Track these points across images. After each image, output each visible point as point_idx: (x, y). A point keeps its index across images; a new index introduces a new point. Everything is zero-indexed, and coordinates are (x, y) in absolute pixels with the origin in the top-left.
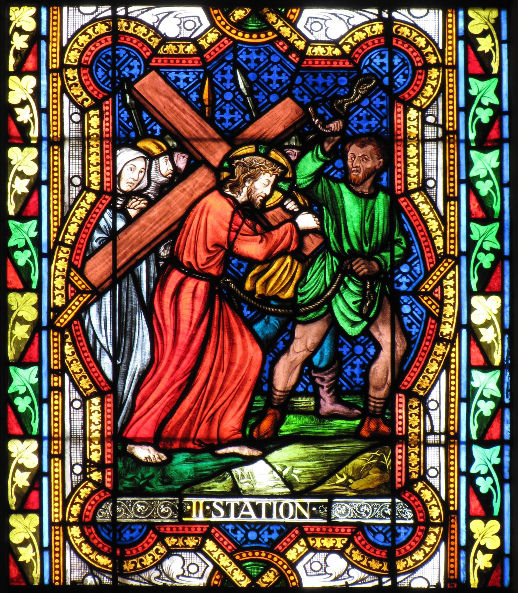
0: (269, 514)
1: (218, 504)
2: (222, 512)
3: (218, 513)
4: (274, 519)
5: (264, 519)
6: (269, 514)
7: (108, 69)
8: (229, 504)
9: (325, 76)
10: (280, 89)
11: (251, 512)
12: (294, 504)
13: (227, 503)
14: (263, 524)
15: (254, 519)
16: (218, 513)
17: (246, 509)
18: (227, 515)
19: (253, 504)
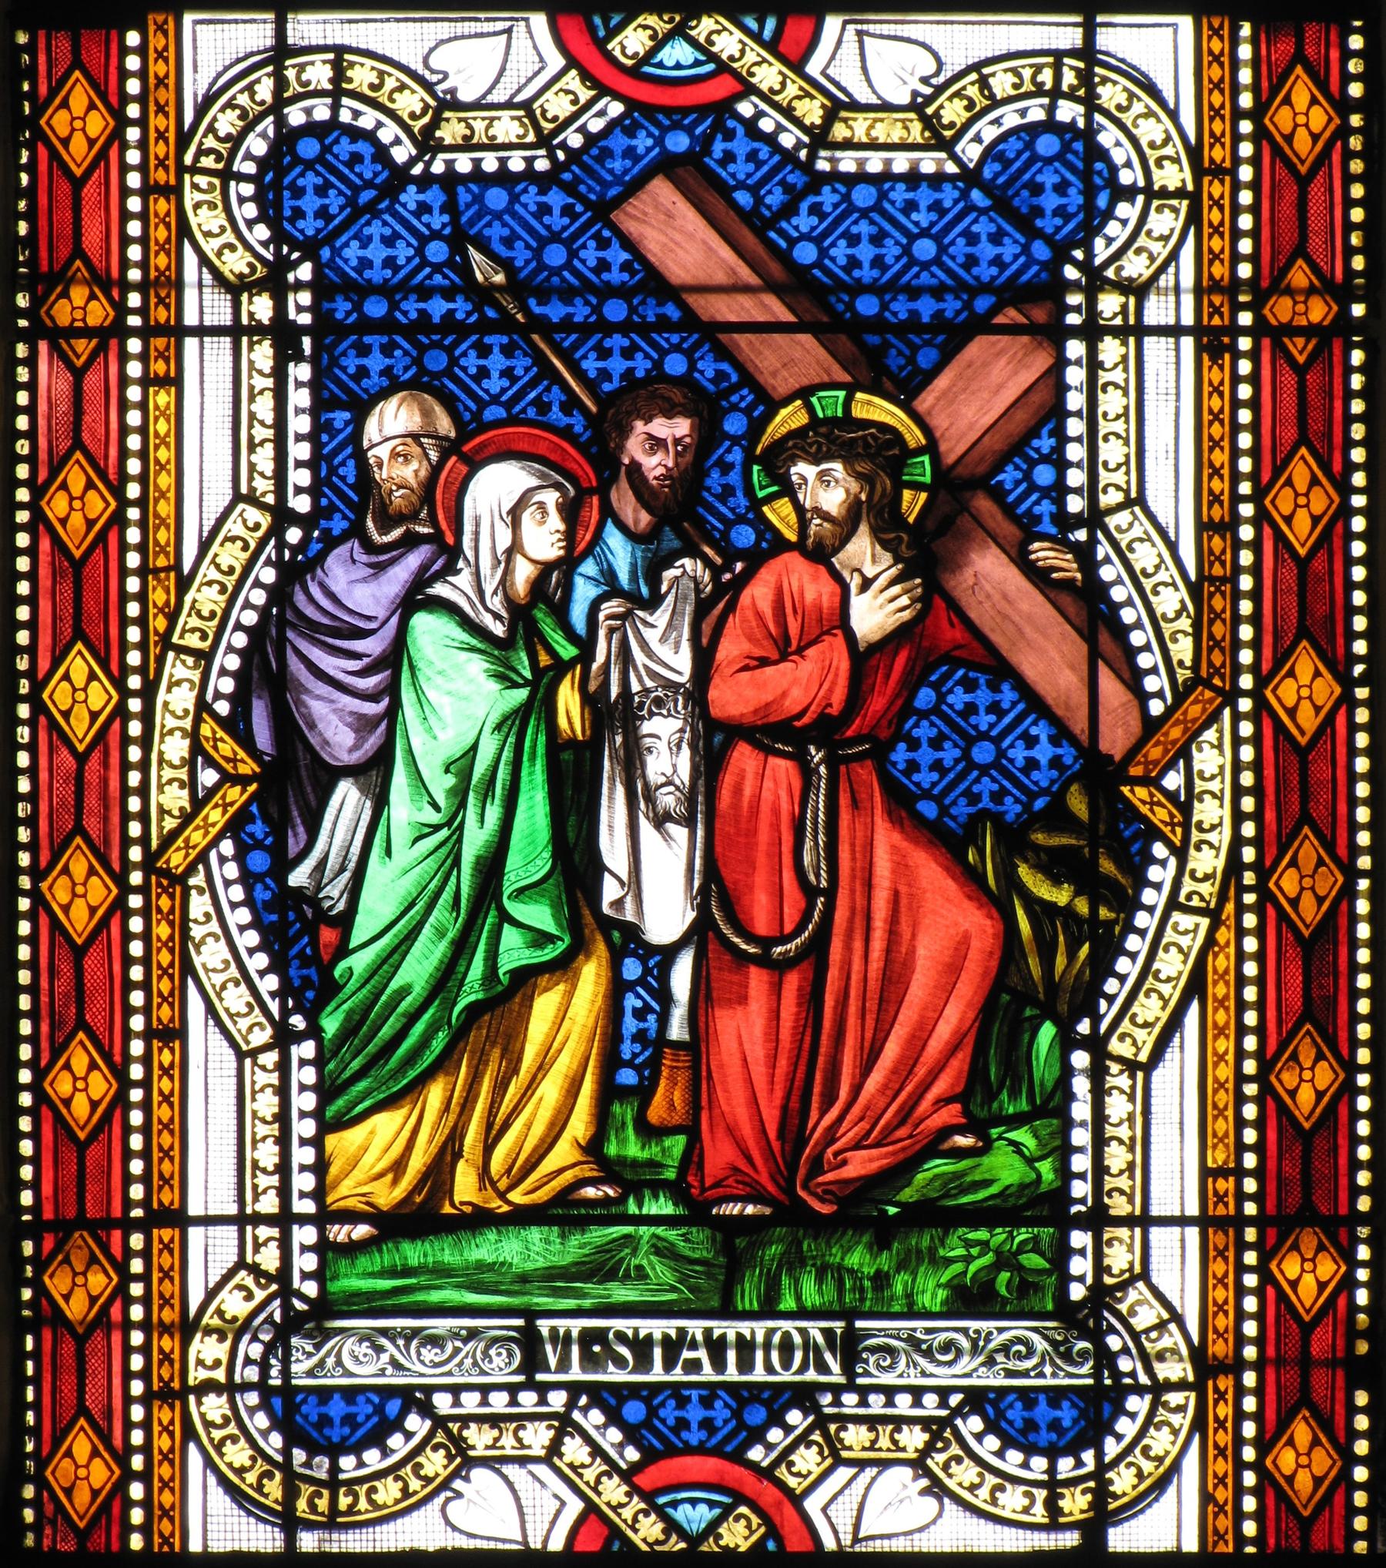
0: (745, 1365)
4: (759, 1375)
5: (732, 1374)
6: (745, 1365)
7: (509, 405)
9: (707, 1403)
13: (642, 1335)
14: (731, 1388)
15: (708, 1374)
16: (620, 1362)
19: (708, 1332)
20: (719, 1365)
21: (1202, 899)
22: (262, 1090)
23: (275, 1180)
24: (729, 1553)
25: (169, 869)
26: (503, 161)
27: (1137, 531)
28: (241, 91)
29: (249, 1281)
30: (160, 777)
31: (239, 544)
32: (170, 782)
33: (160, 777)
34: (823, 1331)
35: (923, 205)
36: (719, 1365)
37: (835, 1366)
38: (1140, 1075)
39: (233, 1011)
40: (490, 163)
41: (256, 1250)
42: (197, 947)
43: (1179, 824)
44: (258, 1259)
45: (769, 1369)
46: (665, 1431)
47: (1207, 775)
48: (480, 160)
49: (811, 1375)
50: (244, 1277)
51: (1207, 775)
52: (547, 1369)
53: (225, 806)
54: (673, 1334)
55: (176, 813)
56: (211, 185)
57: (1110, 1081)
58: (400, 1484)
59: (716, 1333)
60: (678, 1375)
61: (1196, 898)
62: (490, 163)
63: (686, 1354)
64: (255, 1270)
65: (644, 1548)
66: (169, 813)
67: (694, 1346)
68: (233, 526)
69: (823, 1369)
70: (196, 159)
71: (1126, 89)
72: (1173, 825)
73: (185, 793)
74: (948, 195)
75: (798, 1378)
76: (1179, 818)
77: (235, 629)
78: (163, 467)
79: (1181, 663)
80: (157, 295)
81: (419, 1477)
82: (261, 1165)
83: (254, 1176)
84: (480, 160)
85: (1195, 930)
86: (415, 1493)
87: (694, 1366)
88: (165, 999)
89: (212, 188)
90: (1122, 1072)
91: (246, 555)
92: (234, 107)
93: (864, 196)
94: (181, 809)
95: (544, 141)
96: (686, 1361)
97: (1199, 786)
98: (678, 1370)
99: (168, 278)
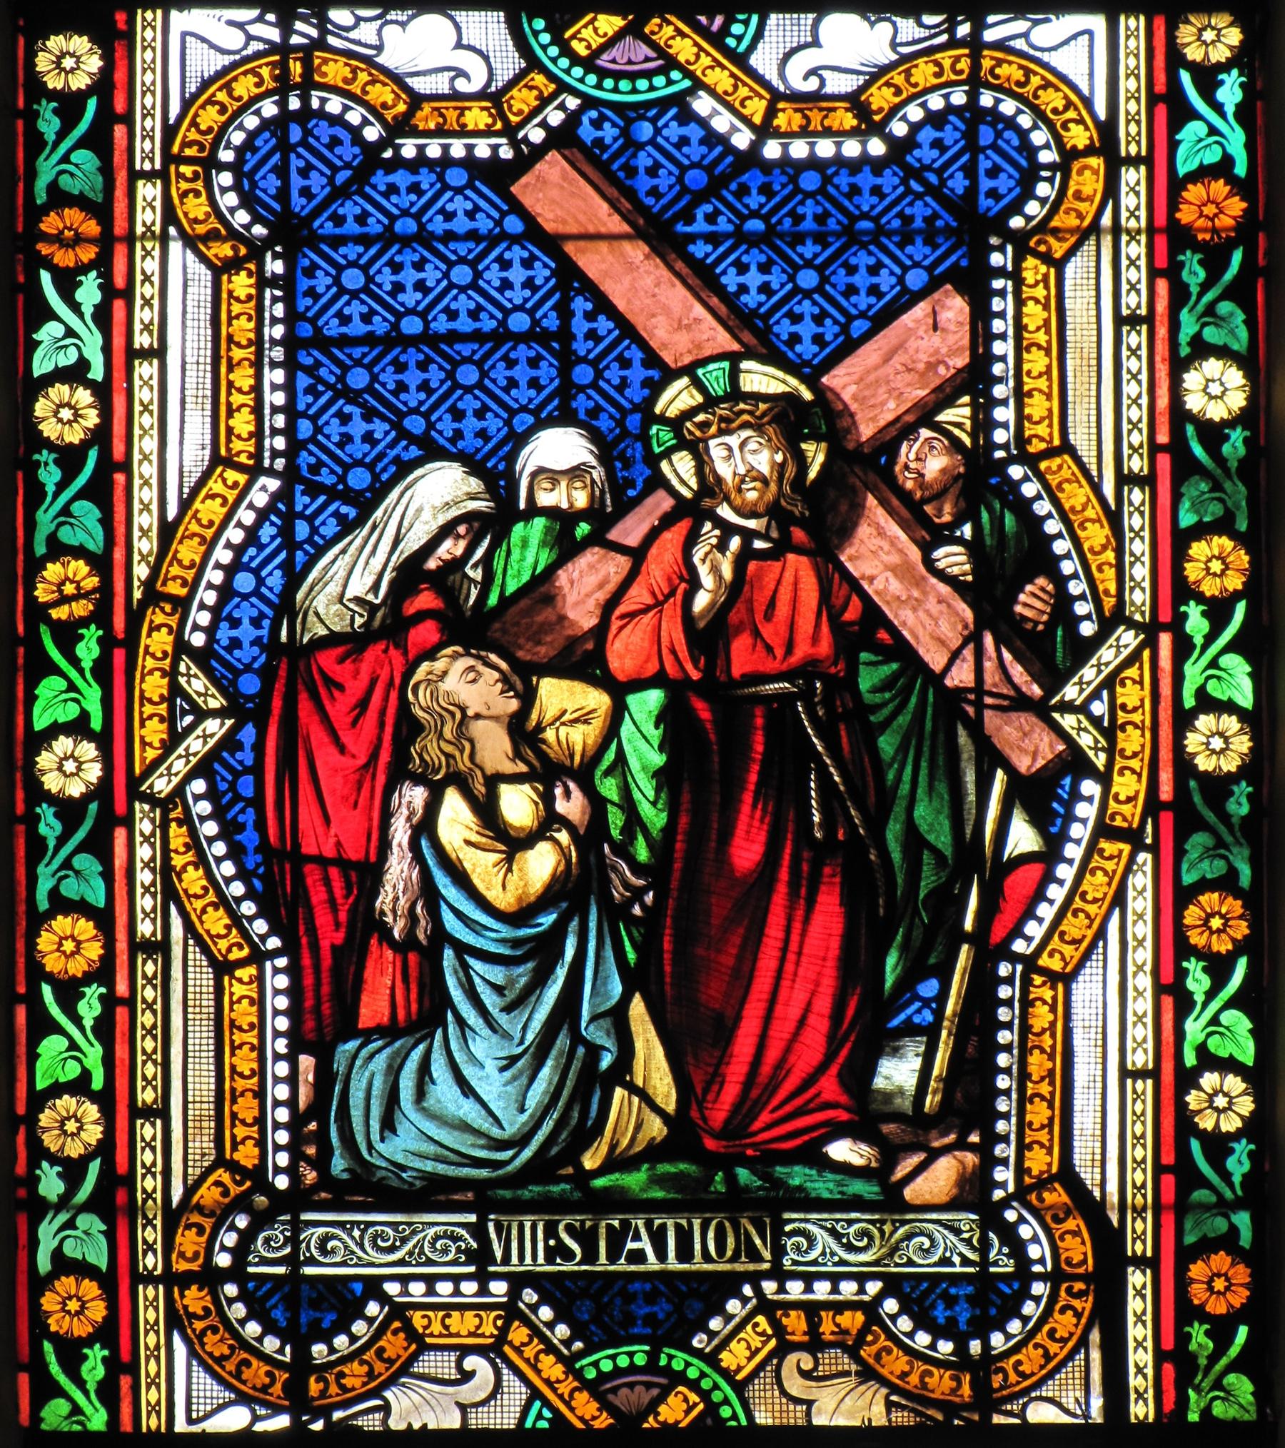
0: (685, 1253)
1: (570, 1229)
3: (568, 1255)
4: (698, 1265)
5: (673, 1264)
6: (685, 1253)
10: (880, 208)
11: (646, 1245)
15: (652, 1263)
17: (637, 1237)
19: (649, 1224)
20: (661, 1255)
21: (1125, 819)
22: (239, 1001)
23: (248, 399)
24: (669, 1429)
25: (152, 794)
26: (470, 148)
28: (220, 89)
29: (226, 1177)
30: (141, 713)
31: (219, 500)
32: (150, 717)
33: (141, 713)
35: (863, 270)
36: (661, 1255)
37: (767, 1255)
38: (1060, 987)
39: (213, 932)
40: (458, 150)
41: (234, 1148)
42: (179, 875)
43: (1103, 749)
44: (236, 1156)
45: (707, 1257)
46: (620, 349)
47: (1130, 707)
48: (449, 145)
49: (744, 1266)
50: (223, 1175)
51: (1130, 707)
52: (495, 1263)
53: (205, 737)
54: (616, 1223)
55: (157, 744)
56: (195, 173)
57: (1034, 993)
58: (368, 88)
59: (657, 1222)
60: (622, 1266)
61: (1118, 818)
62: (458, 150)
63: (631, 1245)
64: (233, 1167)
65: (580, 1425)
66: (150, 745)
67: (637, 1237)
68: (215, 486)
70: (181, 150)
71: (1033, 1374)
72: (1096, 749)
73: (164, 726)
74: (889, 180)
75: (728, 1267)
76: (1103, 743)
77: (218, 865)
78: (149, 1032)
79: (1107, 592)
80: (144, 248)
81: (383, 1360)
82: (236, 339)
83: (229, 349)
84: (449, 145)
85: (1119, 856)
86: (380, 1374)
87: (638, 1256)
88: (149, 1083)
89: (196, 176)
90: (1044, 984)
91: (224, 510)
92: (214, 103)
93: (810, 181)
94: (162, 741)
95: (510, 131)
97: (1122, 717)
98: (622, 1261)
99: (153, 233)
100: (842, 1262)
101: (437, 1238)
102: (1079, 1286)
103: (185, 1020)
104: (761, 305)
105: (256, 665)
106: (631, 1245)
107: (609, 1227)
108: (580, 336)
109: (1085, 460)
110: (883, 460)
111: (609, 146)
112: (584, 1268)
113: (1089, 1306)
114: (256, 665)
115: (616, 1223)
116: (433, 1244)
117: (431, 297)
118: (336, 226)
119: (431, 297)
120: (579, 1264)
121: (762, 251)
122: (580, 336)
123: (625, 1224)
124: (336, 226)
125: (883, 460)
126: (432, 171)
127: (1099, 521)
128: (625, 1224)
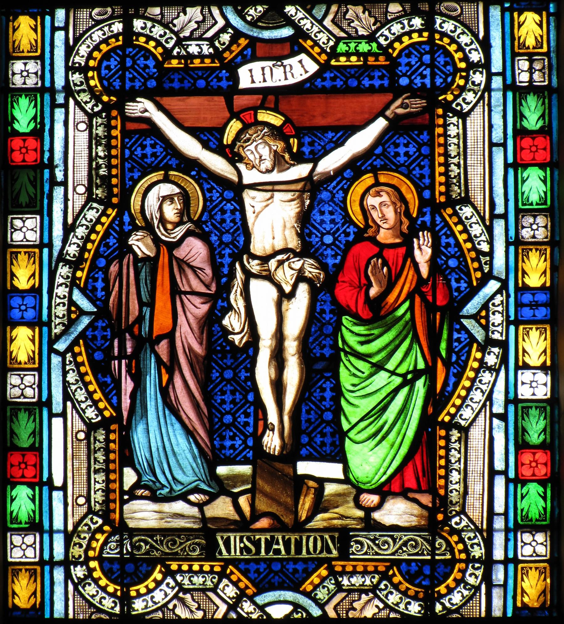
2: (253, 549)
6: (299, 550)
8: (289, 539)
11: (281, 547)
12: (322, 538)
17: (278, 543)
18: (258, 552)
19: (283, 538)
27: (90, 105)
34: (330, 537)
45: (308, 552)
49: (324, 555)
54: (268, 537)
59: (287, 537)
65: (245, 615)
67: (278, 543)
69: (329, 551)
87: (278, 552)
96: (274, 549)
98: (271, 553)
100: (377, 554)
101: (190, 545)
102: (477, 565)
103: (73, 488)
104: (398, 138)
105: (374, 157)
106: (275, 547)
107: (266, 539)
108: (100, 280)
109: (479, 208)
110: (430, 430)
111: (117, 154)
112: (255, 557)
113: (481, 573)
114: (374, 157)
115: (268, 537)
116: (189, 547)
117: (392, 141)
118: (129, 169)
119: (392, 141)
120: (254, 555)
121: (405, 138)
122: (100, 280)
123: (272, 537)
124: (129, 169)
125: (430, 430)
126: (429, 140)
127: (478, 223)
128: (272, 537)
